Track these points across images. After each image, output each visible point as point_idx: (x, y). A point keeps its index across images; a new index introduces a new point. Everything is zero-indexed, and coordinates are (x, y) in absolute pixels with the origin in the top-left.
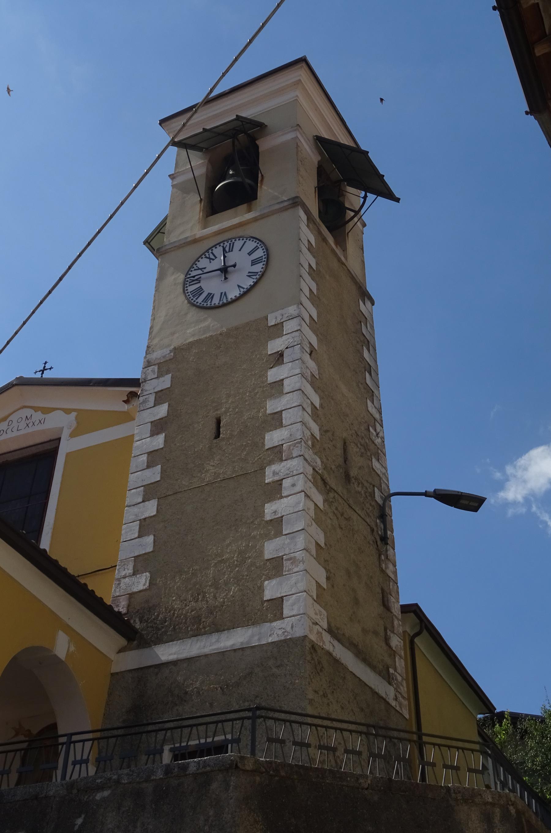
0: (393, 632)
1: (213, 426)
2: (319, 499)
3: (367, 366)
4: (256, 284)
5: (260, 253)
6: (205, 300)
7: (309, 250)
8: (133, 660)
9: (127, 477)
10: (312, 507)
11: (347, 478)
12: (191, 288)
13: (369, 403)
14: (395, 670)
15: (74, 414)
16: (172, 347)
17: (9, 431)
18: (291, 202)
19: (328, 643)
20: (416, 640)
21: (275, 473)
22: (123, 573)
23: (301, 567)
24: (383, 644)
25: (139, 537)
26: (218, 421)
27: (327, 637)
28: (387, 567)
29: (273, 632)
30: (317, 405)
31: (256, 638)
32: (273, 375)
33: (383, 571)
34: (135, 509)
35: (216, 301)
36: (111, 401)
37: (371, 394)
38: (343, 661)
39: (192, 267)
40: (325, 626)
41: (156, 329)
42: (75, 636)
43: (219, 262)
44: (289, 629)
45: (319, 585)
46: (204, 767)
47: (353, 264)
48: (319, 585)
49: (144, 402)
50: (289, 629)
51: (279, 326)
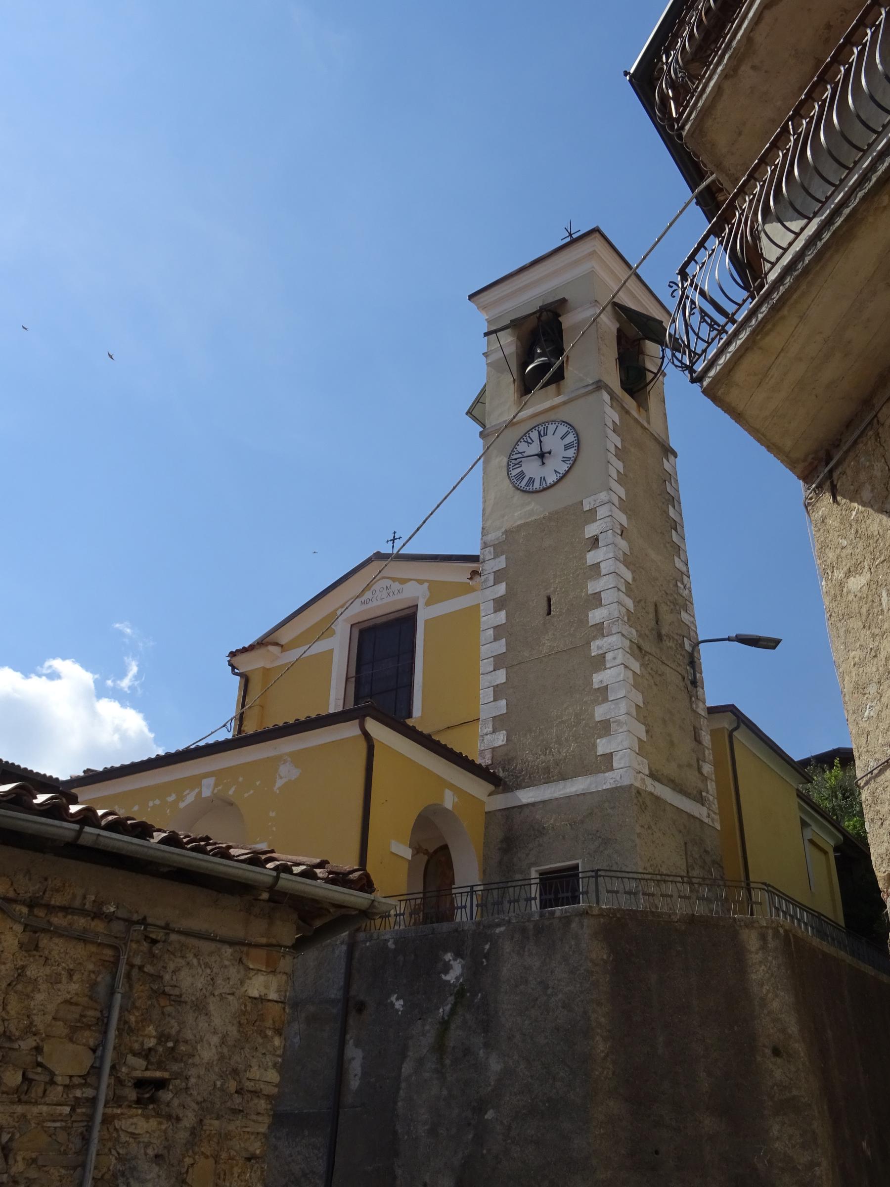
0: (704, 761)
1: (545, 603)
2: (636, 666)
3: (673, 524)
4: (570, 468)
5: (571, 438)
6: (527, 485)
7: (614, 431)
8: (500, 802)
9: (479, 649)
10: (630, 674)
11: (660, 637)
12: (514, 473)
13: (676, 559)
14: (707, 793)
15: (426, 585)
16: (503, 530)
17: (374, 599)
18: (594, 386)
19: (652, 786)
20: (735, 733)
21: (599, 648)
22: (485, 731)
23: (625, 728)
24: (697, 773)
25: (494, 701)
26: (549, 600)
27: (649, 781)
28: (697, 707)
29: (607, 781)
30: (630, 581)
31: (594, 786)
32: (592, 557)
33: (694, 711)
34: (488, 677)
35: (537, 485)
36: (458, 574)
37: (678, 550)
38: (663, 797)
39: (513, 451)
40: (647, 772)
41: (488, 511)
42: (459, 791)
43: (534, 449)
44: (618, 778)
45: (640, 740)
46: (566, 912)
47: (655, 427)
48: (640, 740)
49: (485, 581)
50: (618, 778)
51: (593, 511)
